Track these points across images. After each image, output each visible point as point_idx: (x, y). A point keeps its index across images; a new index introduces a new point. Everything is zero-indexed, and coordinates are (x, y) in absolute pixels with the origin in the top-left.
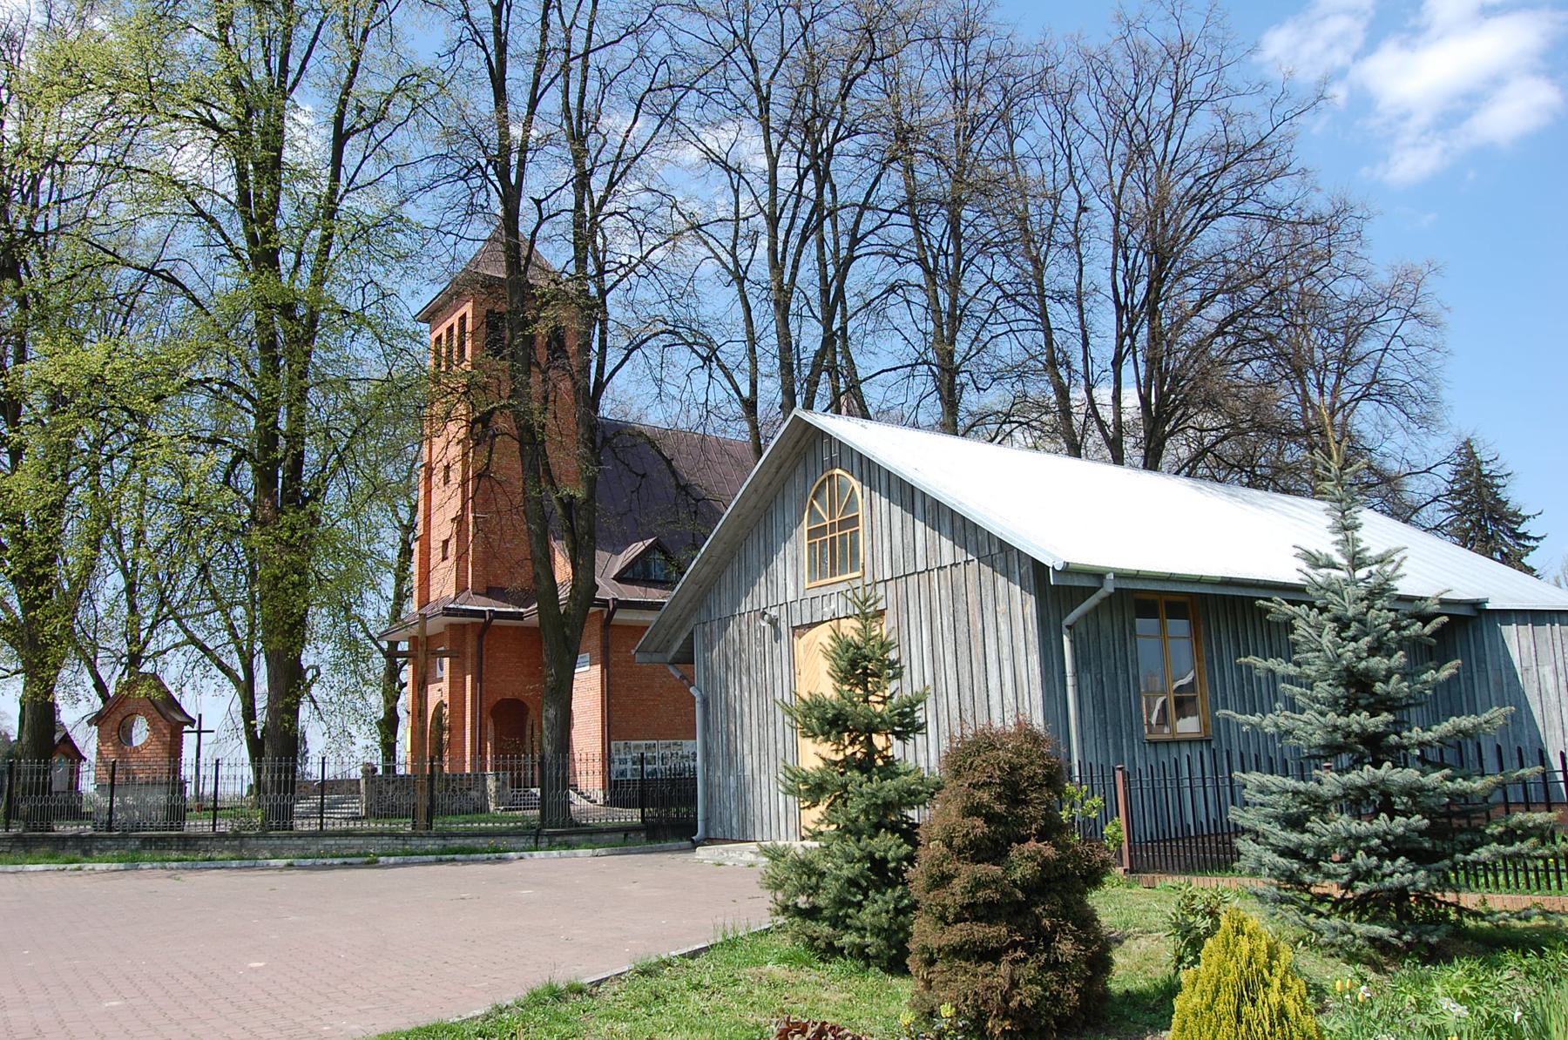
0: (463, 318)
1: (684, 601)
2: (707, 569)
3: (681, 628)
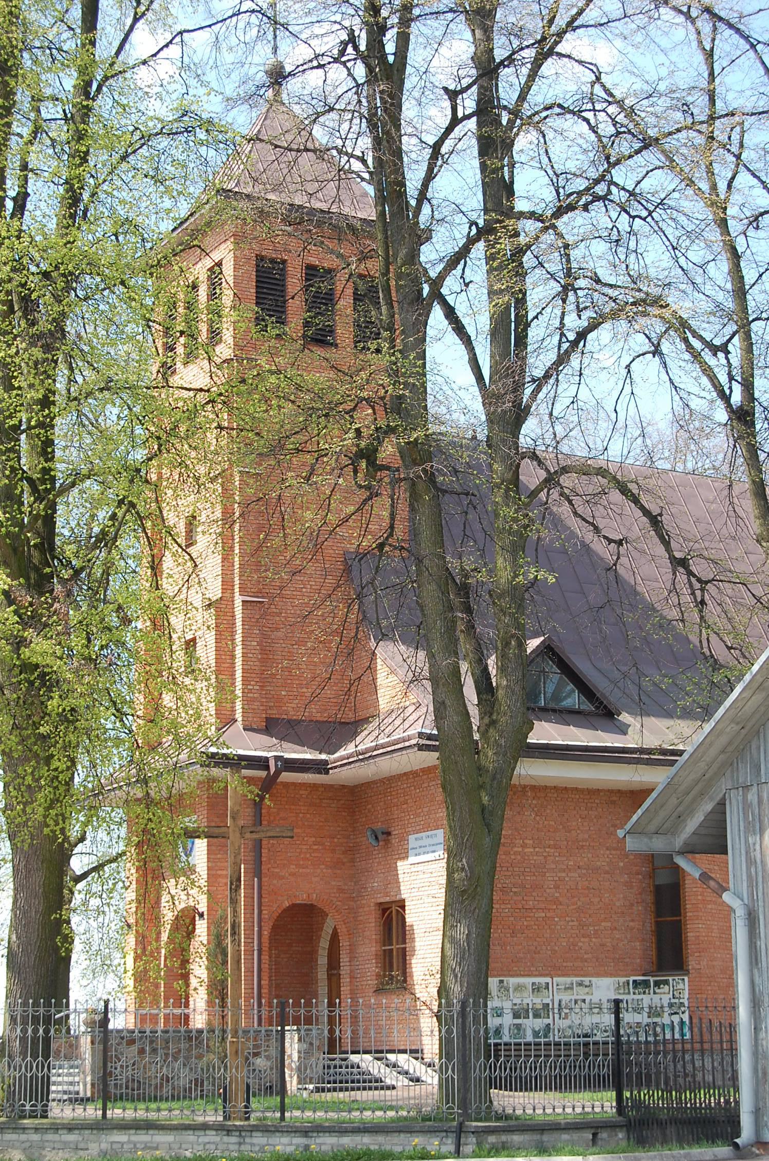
0: (216, 270)
1: (713, 752)
2: (758, 698)
3: (702, 794)
